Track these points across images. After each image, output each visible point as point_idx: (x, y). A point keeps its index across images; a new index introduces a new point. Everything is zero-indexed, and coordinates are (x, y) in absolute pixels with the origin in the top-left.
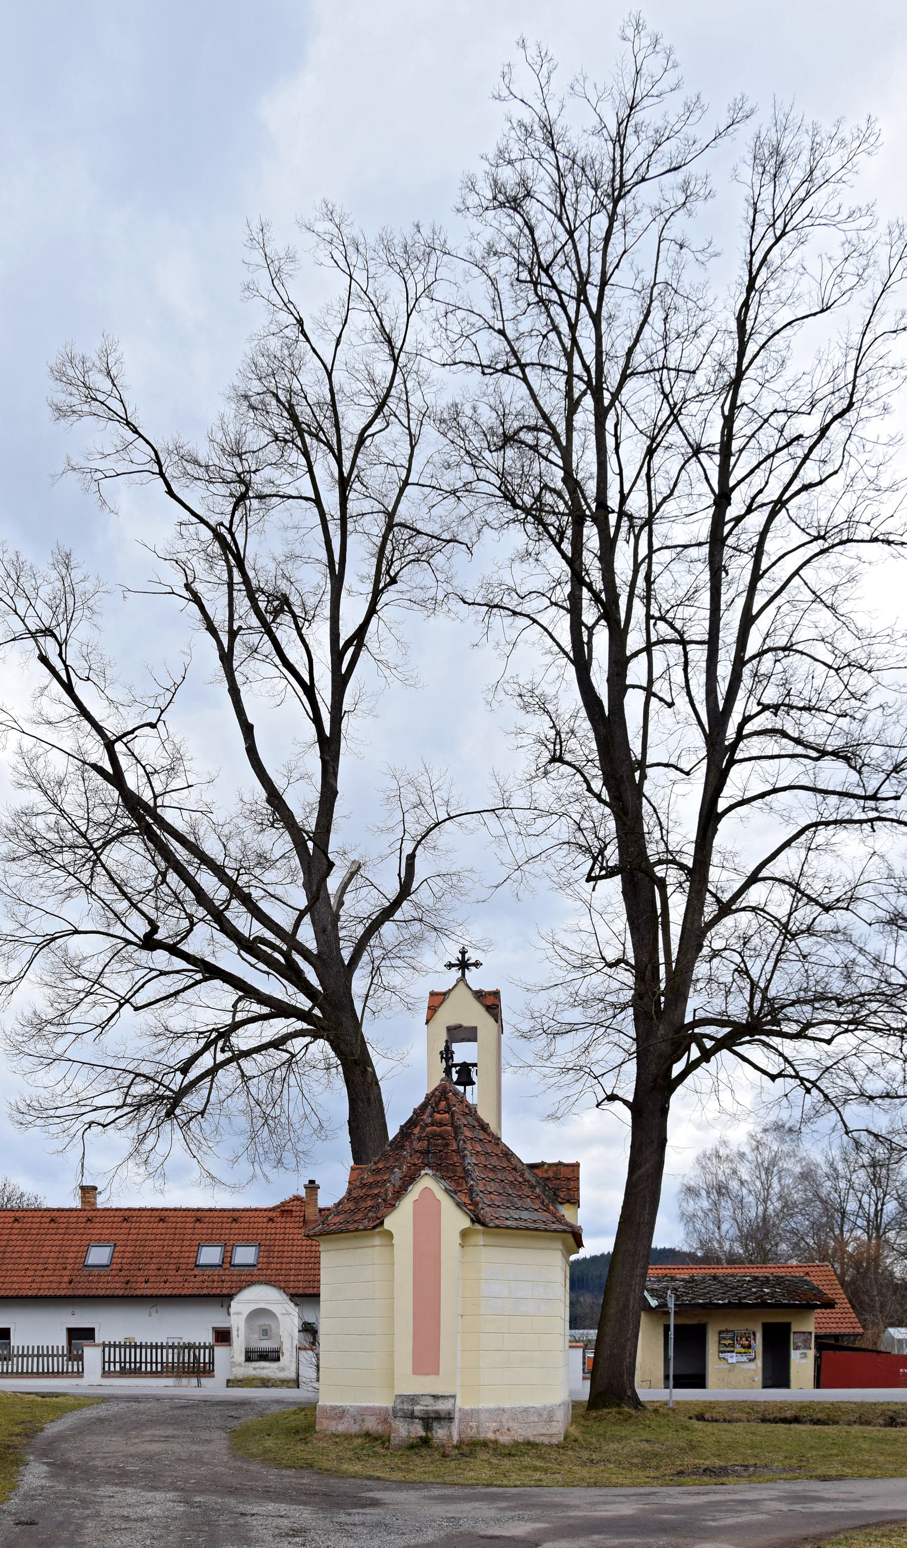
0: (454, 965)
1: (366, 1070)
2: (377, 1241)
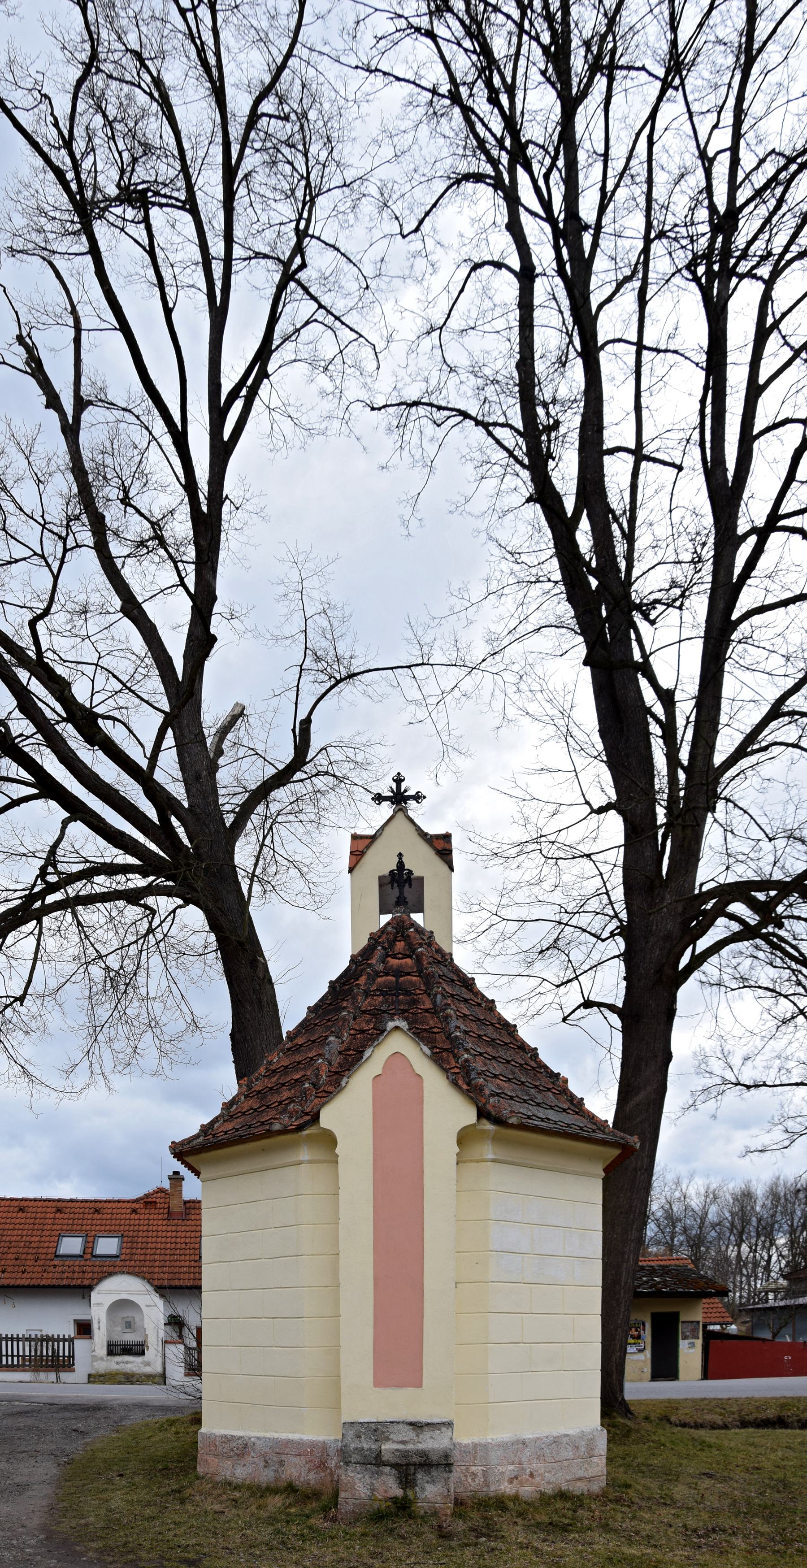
0: (386, 799)
1: (256, 961)
2: (304, 1154)
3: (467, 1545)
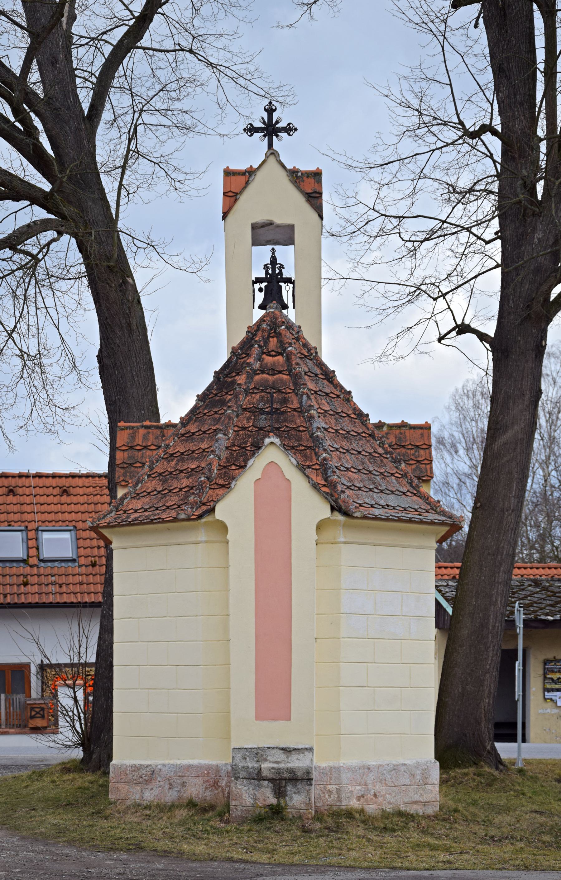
0: (257, 130)
1: (125, 282)
2: (202, 536)
3: (321, 836)
